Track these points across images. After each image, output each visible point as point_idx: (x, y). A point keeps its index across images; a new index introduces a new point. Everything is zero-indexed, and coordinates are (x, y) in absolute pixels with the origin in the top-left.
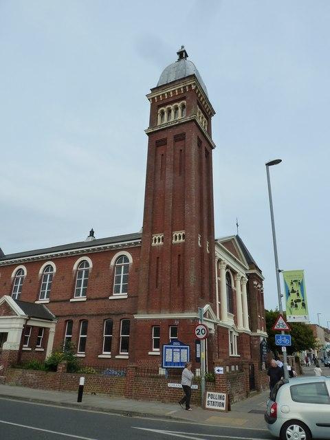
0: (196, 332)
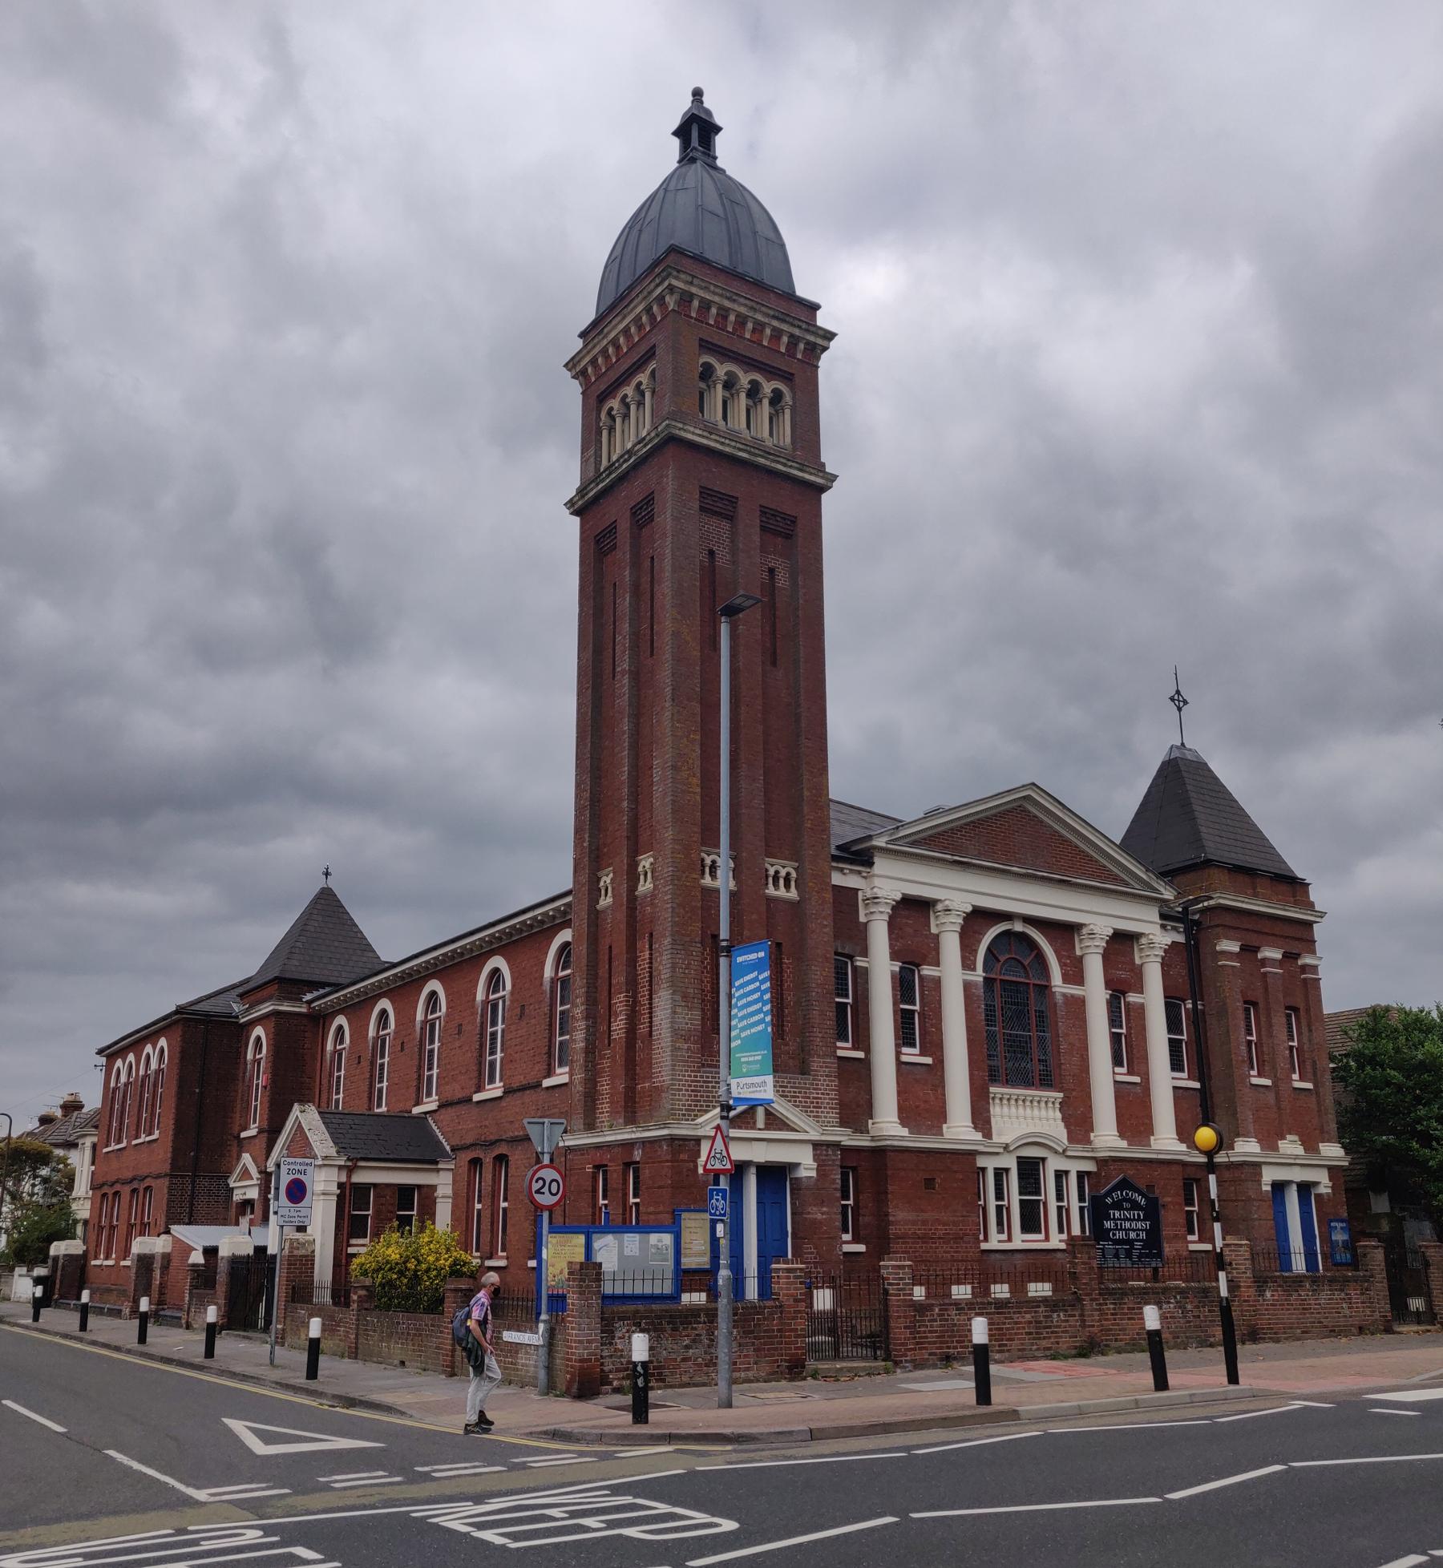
0: (536, 1186)
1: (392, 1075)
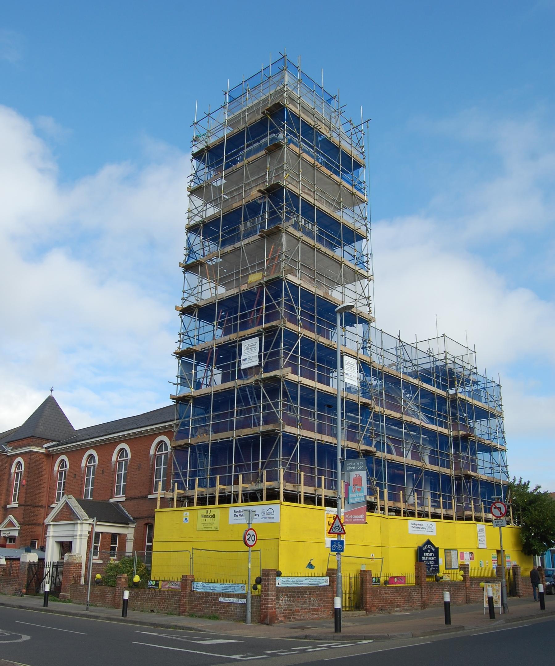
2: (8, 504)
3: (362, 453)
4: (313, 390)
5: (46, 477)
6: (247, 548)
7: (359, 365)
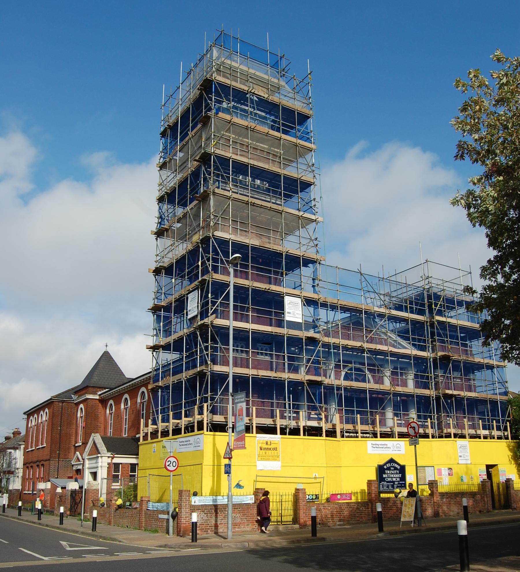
1: (129, 423)
2: (77, 443)
3: (307, 383)
4: (247, 331)
5: (102, 419)
6: (168, 473)
7: (304, 303)
